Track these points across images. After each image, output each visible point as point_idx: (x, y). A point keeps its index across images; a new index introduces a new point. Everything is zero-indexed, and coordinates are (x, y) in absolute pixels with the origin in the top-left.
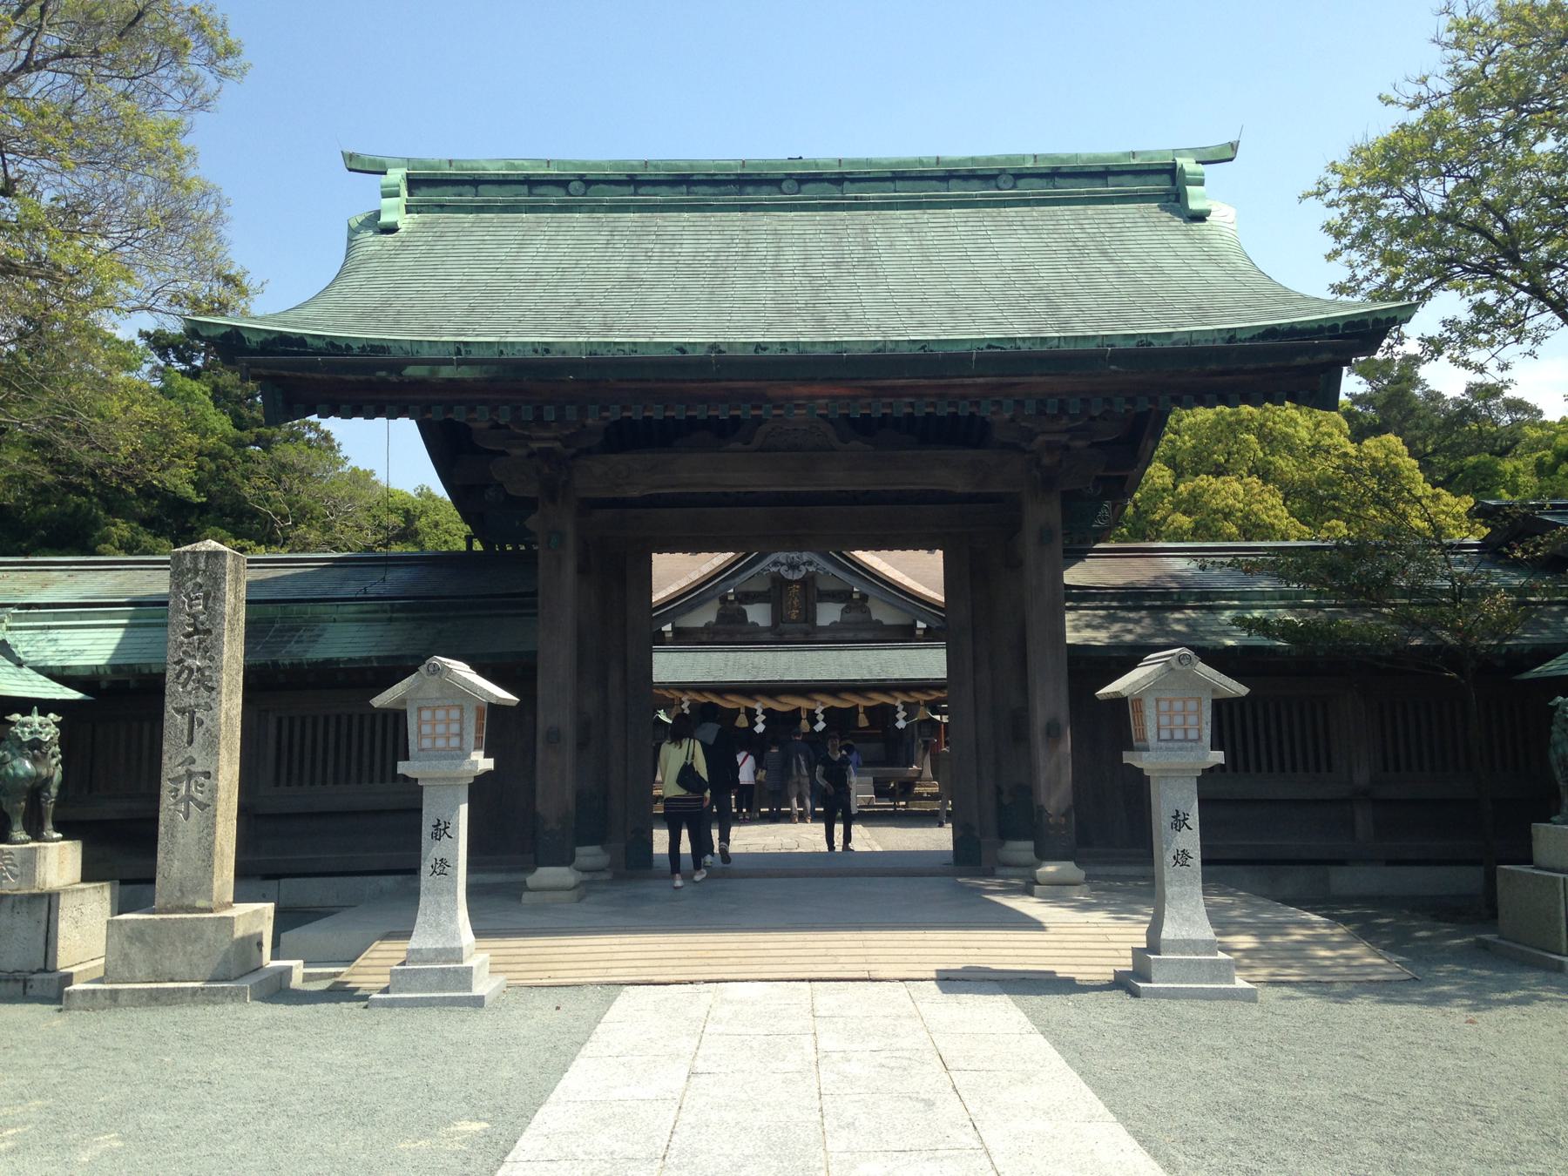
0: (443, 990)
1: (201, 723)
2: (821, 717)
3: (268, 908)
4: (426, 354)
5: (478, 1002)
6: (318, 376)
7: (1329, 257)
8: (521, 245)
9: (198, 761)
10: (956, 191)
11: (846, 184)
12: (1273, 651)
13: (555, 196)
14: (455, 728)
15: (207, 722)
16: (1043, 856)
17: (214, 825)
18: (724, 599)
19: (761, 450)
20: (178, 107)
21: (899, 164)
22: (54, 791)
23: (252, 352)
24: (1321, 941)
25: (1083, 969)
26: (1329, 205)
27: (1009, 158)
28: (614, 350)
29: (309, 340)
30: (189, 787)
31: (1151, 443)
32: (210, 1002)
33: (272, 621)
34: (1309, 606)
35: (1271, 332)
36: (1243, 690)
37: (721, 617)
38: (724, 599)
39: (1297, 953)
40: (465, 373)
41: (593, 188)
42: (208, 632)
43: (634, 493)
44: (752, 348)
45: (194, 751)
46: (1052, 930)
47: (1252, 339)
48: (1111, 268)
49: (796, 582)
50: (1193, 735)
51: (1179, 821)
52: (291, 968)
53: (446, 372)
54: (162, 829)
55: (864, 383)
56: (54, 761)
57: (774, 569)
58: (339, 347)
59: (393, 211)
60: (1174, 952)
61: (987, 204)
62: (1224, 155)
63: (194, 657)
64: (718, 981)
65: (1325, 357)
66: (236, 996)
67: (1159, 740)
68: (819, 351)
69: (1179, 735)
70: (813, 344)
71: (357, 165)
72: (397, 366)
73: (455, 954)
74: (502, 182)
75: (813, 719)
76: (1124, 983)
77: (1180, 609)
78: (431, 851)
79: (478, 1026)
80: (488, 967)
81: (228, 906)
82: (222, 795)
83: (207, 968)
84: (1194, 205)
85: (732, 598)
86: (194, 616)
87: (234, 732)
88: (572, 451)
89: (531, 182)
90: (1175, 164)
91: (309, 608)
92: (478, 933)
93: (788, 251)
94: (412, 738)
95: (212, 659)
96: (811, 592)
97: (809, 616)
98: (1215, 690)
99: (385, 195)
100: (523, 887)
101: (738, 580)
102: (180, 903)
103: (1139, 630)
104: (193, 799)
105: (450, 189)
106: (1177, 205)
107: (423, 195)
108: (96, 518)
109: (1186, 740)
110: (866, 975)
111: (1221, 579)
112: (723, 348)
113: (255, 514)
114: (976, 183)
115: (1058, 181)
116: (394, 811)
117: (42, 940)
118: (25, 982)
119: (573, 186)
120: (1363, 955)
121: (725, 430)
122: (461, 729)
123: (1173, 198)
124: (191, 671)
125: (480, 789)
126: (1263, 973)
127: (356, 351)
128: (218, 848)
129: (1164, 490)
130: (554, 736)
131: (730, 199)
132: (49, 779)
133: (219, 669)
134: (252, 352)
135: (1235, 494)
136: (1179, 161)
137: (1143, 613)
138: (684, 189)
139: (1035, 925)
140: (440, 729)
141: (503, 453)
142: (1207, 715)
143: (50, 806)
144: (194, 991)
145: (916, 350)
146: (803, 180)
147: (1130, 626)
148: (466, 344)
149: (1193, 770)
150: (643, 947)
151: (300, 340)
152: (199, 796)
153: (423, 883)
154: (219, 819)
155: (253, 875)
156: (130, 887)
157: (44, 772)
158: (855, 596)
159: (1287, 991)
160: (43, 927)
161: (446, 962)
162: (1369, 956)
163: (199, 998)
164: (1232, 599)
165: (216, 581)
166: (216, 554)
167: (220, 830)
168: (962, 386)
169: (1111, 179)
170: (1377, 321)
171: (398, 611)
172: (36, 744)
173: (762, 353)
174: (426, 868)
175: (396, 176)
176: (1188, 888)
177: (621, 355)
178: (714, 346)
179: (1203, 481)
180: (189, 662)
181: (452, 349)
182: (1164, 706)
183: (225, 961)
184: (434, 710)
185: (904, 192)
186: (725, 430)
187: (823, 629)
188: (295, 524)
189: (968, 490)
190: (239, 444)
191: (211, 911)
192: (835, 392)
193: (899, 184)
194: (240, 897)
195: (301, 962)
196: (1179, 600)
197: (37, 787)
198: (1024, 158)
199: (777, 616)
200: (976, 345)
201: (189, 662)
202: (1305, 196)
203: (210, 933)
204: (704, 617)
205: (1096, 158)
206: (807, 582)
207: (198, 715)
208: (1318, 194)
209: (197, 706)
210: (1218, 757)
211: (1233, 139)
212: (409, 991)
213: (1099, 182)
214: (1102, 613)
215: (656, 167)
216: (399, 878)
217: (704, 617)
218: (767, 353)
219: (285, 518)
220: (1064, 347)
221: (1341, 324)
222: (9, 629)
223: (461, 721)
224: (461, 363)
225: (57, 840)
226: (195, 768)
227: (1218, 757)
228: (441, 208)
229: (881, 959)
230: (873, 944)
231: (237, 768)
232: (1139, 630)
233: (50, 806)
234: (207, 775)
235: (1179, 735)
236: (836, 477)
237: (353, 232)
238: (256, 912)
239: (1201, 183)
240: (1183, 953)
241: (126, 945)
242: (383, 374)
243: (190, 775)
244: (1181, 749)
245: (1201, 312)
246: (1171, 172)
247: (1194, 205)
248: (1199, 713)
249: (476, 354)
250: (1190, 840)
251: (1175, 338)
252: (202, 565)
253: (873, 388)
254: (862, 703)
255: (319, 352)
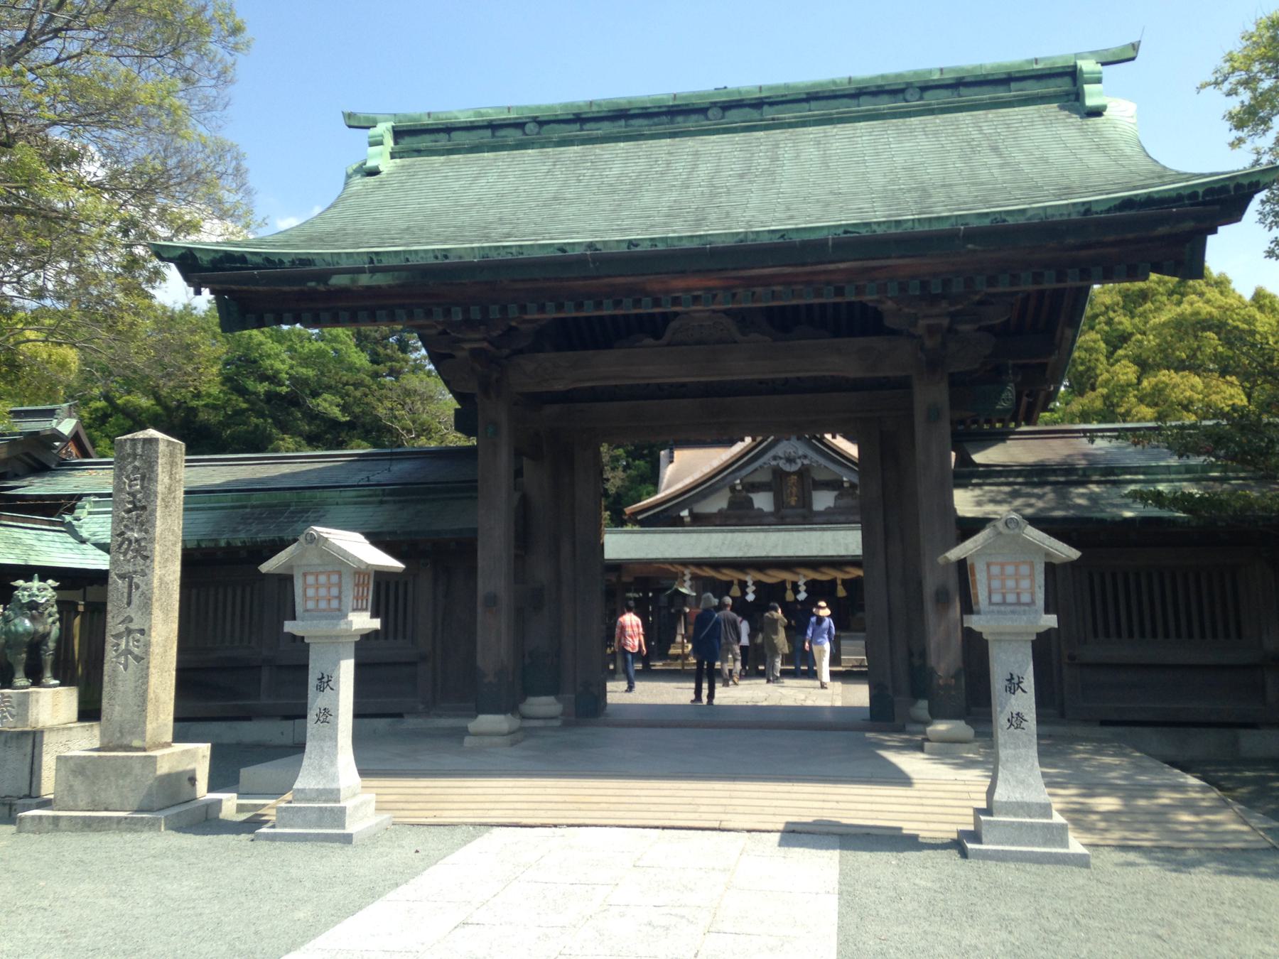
0: (320, 827)
1: (138, 587)
2: (803, 588)
3: (204, 749)
4: (345, 264)
5: (347, 839)
6: (260, 288)
7: (1232, 145)
8: (476, 178)
9: (135, 620)
10: (866, 105)
11: (766, 108)
12: (1172, 522)
13: (516, 134)
14: (335, 591)
15: (143, 586)
16: (938, 713)
17: (147, 675)
18: (733, 489)
19: (669, 345)
20: (213, 82)
21: (814, 86)
22: (51, 645)
23: (207, 270)
24: (1189, 806)
25: (932, 826)
26: (1229, 94)
27: (916, 73)
28: (503, 252)
29: (248, 257)
30: (127, 642)
31: (1069, 332)
32: (130, 830)
33: (288, 505)
34: (1214, 479)
35: (1128, 203)
36: (1074, 554)
37: (732, 504)
38: (733, 489)
39: (1160, 817)
40: (380, 280)
41: (546, 127)
42: (144, 508)
43: (559, 386)
44: (625, 245)
45: (132, 612)
46: (917, 786)
47: (1109, 211)
48: (998, 161)
49: (794, 473)
50: (1025, 598)
51: (1013, 684)
52: (220, 801)
53: (364, 280)
54: (106, 678)
55: (734, 274)
56: (50, 620)
57: (774, 463)
58: (273, 262)
59: (380, 158)
60: (1007, 814)
61: (895, 115)
62: (1125, 56)
63: (132, 530)
64: (579, 826)
65: (1189, 225)
66: (152, 825)
67: (990, 603)
68: (687, 245)
69: (1011, 598)
70: (680, 238)
71: (357, 122)
72: (324, 276)
73: (333, 795)
74: (470, 127)
75: (796, 590)
76: (958, 845)
77: (1083, 483)
78: (316, 702)
79: (334, 860)
80: (373, 805)
81: (168, 745)
82: (156, 650)
83: (134, 800)
84: (1090, 102)
85: (739, 488)
86: (133, 495)
87: (170, 596)
88: (506, 351)
89: (493, 126)
90: (1075, 66)
91: (318, 493)
92: (363, 773)
93: (702, 167)
94: (298, 600)
95: (146, 532)
96: (807, 481)
97: (806, 502)
98: (1048, 554)
99: (372, 144)
100: (464, 732)
101: (744, 473)
102: (119, 742)
103: (1040, 504)
104: (131, 653)
105: (428, 137)
106: (1077, 104)
107: (407, 142)
108: (270, 434)
109: (1019, 603)
110: (716, 825)
111: (1131, 455)
112: (599, 246)
113: (390, 430)
114: (885, 98)
115: (963, 90)
116: (386, 664)
117: (27, 770)
118: (11, 805)
119: (531, 127)
120: (1231, 824)
121: (654, 326)
122: (340, 592)
123: (1072, 97)
124: (130, 542)
125: (365, 642)
126: (1115, 836)
127: (287, 264)
128: (151, 695)
129: (1129, 385)
130: (492, 600)
131: (661, 129)
132: (46, 636)
133: (152, 541)
134: (207, 270)
135: (1193, 388)
136: (1080, 63)
137: (1048, 489)
138: (623, 122)
139: (903, 780)
140: (323, 592)
141: (451, 356)
142: (1040, 579)
143: (48, 658)
144: (119, 820)
145: (776, 239)
146: (727, 106)
147: (1033, 501)
148: (377, 253)
149: (1028, 634)
150: (531, 791)
151: (242, 258)
152: (136, 651)
153: (309, 730)
154: (152, 670)
155: (188, 722)
156: (366, 721)
157: (41, 629)
158: (846, 485)
159: (1132, 857)
160: (28, 760)
161: (325, 801)
162: (1235, 822)
163: (123, 826)
164: (1137, 473)
165: (151, 464)
166: (151, 441)
167: (154, 680)
168: (825, 272)
169: (1013, 85)
170: (1239, 187)
171: (389, 495)
172: (33, 606)
173: (634, 249)
174: (312, 716)
175: (383, 129)
176: (1023, 751)
177: (510, 257)
178: (591, 245)
179: (1164, 376)
180: (129, 534)
181: (366, 259)
182: (995, 570)
183: (149, 794)
184: (317, 575)
185: (817, 110)
186: (654, 326)
187: (820, 513)
188: (418, 436)
189: (860, 374)
190: (376, 375)
191: (144, 750)
192: (711, 283)
193: (813, 104)
194: (179, 737)
195: (235, 795)
196: (1084, 475)
197: (35, 643)
198: (930, 72)
199: (779, 502)
200: (833, 231)
201: (129, 534)
202: (1203, 86)
203: (137, 769)
204: (718, 503)
205: (1000, 66)
206: (803, 473)
207: (135, 580)
208: (1216, 83)
209: (135, 572)
210: (1051, 621)
211: (1134, 40)
212: (292, 826)
213: (1001, 88)
214: (1007, 489)
215: (599, 105)
216: (389, 720)
217: (718, 503)
218: (638, 249)
219: (409, 432)
220: (918, 228)
221: (1201, 191)
222: (90, 513)
223: (339, 585)
224: (374, 271)
225: (55, 686)
226: (133, 626)
227: (1051, 621)
228: (419, 152)
229: (740, 809)
230: (739, 794)
231: (175, 626)
232: (1040, 504)
233: (48, 658)
234: (142, 632)
235: (1011, 598)
236: (742, 365)
237: (349, 177)
238: (187, 751)
239: (1099, 81)
240: (1016, 815)
241: (71, 778)
242: (312, 284)
243: (129, 632)
244: (1013, 612)
245: (1068, 191)
246: (1072, 74)
247: (1090, 102)
248: (1032, 577)
249: (386, 262)
250: (1025, 702)
251: (1029, 214)
252: (139, 451)
253: (742, 278)
254: (840, 576)
255: (257, 267)
